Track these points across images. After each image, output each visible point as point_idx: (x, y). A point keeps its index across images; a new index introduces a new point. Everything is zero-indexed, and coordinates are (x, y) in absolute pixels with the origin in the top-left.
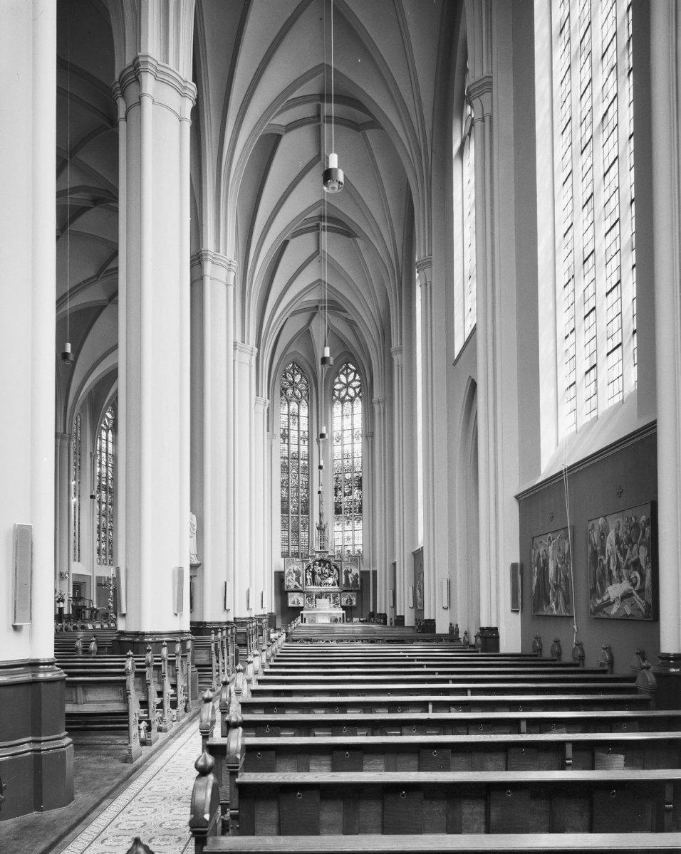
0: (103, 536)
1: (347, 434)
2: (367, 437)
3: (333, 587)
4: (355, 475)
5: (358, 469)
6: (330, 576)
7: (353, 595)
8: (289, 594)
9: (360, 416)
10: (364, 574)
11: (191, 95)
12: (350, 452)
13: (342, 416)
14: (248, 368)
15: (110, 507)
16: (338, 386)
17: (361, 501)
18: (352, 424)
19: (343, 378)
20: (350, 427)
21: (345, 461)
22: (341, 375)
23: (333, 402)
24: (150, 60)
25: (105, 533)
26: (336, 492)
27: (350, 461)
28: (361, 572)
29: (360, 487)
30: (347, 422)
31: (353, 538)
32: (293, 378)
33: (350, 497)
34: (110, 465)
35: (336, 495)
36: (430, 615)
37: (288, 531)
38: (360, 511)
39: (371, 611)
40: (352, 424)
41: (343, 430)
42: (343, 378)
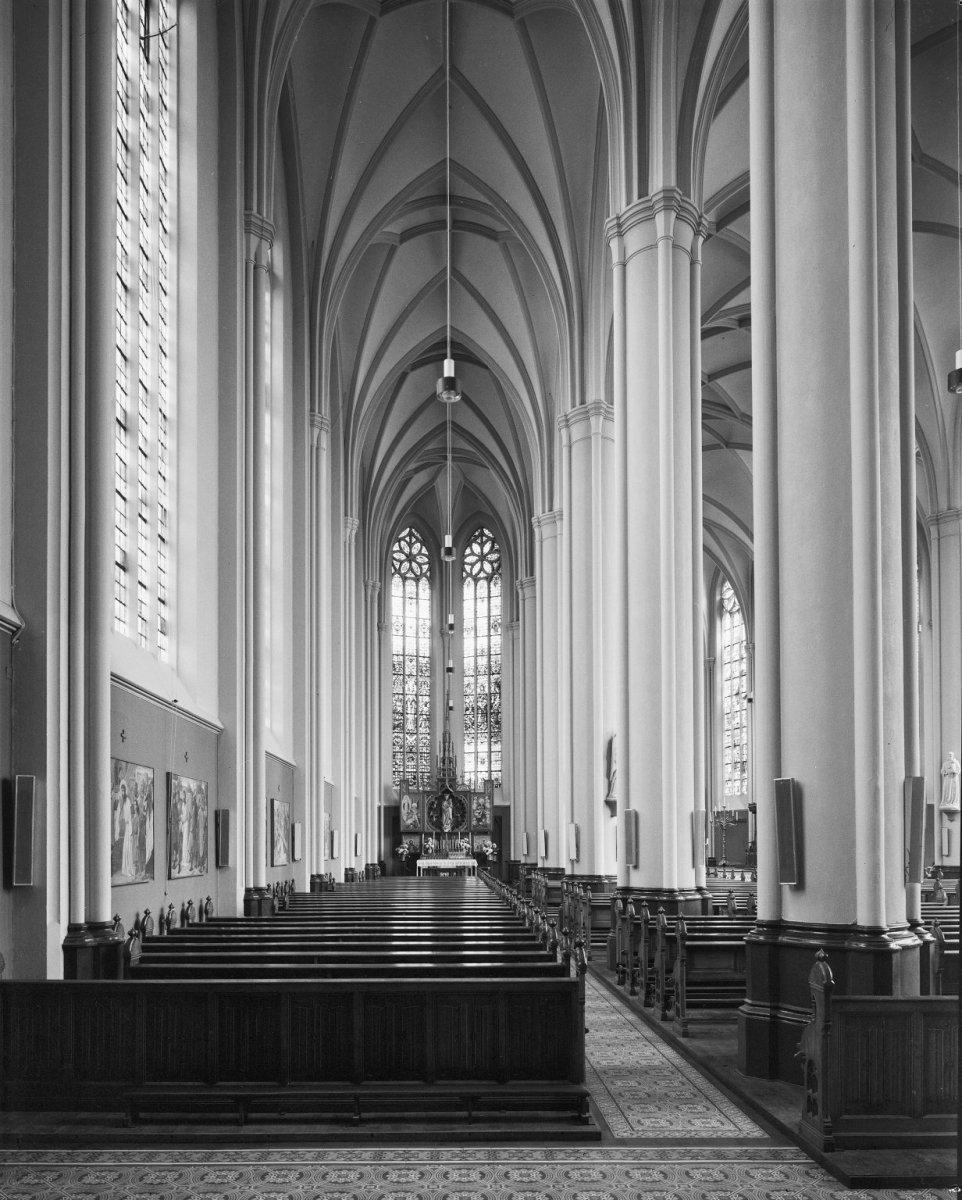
8: (78, 951)
9: (428, 603)
16: (469, 560)
19: (476, 548)
22: (403, 543)
23: (463, 580)
32: (410, 548)
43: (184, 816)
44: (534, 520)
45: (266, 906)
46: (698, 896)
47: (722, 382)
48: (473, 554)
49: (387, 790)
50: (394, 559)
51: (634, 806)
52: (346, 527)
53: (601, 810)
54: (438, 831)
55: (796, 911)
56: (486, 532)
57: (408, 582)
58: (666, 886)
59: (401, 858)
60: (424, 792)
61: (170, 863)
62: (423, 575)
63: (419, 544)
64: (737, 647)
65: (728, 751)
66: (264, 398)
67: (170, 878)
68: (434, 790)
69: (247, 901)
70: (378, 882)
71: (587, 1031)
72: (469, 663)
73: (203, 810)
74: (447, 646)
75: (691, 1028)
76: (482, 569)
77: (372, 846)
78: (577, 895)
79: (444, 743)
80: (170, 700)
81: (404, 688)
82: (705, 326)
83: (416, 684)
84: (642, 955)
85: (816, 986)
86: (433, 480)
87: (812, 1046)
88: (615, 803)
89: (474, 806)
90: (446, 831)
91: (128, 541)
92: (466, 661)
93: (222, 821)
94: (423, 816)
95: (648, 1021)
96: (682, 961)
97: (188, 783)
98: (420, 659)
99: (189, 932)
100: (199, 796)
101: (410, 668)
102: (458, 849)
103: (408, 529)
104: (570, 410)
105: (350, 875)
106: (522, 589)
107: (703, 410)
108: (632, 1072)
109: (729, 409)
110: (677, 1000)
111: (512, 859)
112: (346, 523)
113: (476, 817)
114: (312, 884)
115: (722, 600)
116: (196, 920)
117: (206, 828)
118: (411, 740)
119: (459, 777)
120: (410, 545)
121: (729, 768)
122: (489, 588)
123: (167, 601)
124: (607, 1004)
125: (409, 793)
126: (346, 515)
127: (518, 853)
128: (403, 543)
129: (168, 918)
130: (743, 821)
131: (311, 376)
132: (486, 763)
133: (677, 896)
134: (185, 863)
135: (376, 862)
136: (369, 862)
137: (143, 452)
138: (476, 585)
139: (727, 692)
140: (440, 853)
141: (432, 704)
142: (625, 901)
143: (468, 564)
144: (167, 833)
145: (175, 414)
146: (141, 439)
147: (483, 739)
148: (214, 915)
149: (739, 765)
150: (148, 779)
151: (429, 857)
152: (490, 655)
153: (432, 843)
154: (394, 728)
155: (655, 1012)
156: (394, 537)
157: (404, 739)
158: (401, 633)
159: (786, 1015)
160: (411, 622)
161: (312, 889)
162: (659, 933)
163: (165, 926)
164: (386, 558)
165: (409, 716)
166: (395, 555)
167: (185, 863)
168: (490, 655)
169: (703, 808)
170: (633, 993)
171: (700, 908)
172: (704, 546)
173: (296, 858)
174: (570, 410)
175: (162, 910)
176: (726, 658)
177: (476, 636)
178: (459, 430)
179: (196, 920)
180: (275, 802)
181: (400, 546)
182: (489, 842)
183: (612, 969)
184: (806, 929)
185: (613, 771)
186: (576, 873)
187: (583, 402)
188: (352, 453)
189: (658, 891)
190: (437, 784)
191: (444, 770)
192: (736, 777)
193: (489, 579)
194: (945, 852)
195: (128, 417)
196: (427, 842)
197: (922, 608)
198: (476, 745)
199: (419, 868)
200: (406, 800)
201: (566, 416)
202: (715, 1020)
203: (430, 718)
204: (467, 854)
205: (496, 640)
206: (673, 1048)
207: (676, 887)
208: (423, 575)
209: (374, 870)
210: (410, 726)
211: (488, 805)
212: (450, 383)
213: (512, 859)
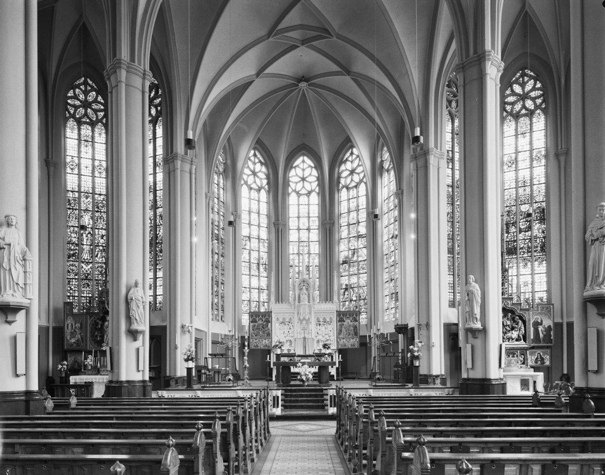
0: (215, 289)
1: (524, 157)
2: (557, 155)
3: (517, 343)
4: (535, 206)
5: (540, 198)
6: (513, 328)
7: (545, 353)
10: (558, 326)
12: (528, 178)
13: (516, 135)
14: (188, 175)
15: (222, 259)
17: (544, 237)
18: (531, 143)
20: (528, 148)
21: (521, 191)
24: (122, 61)
25: (218, 286)
26: (508, 228)
27: (528, 189)
28: (556, 324)
29: (542, 220)
30: (524, 142)
31: (533, 284)
33: (527, 234)
34: (221, 213)
35: (508, 232)
37: (453, 275)
38: (543, 248)
39: (565, 372)
40: (531, 143)
41: (517, 152)
42: (517, 89)
57: (83, 127)
62: (99, 121)
63: (94, 93)
64: (392, 198)
65: (387, 285)
83: (92, 218)
94: (86, 336)
98: (96, 196)
101: (86, 203)
103: (83, 79)
111: (168, 375)
118: (86, 268)
120: (86, 93)
121: (387, 299)
128: (77, 90)
149: (394, 295)
158: (76, 171)
160: (86, 163)
165: (85, 246)
173: (140, 369)
176: (385, 209)
192: (392, 306)
194: (593, 365)
197: (549, 143)
200: (69, 321)
208: (99, 121)
210: (86, 256)
213: (168, 375)
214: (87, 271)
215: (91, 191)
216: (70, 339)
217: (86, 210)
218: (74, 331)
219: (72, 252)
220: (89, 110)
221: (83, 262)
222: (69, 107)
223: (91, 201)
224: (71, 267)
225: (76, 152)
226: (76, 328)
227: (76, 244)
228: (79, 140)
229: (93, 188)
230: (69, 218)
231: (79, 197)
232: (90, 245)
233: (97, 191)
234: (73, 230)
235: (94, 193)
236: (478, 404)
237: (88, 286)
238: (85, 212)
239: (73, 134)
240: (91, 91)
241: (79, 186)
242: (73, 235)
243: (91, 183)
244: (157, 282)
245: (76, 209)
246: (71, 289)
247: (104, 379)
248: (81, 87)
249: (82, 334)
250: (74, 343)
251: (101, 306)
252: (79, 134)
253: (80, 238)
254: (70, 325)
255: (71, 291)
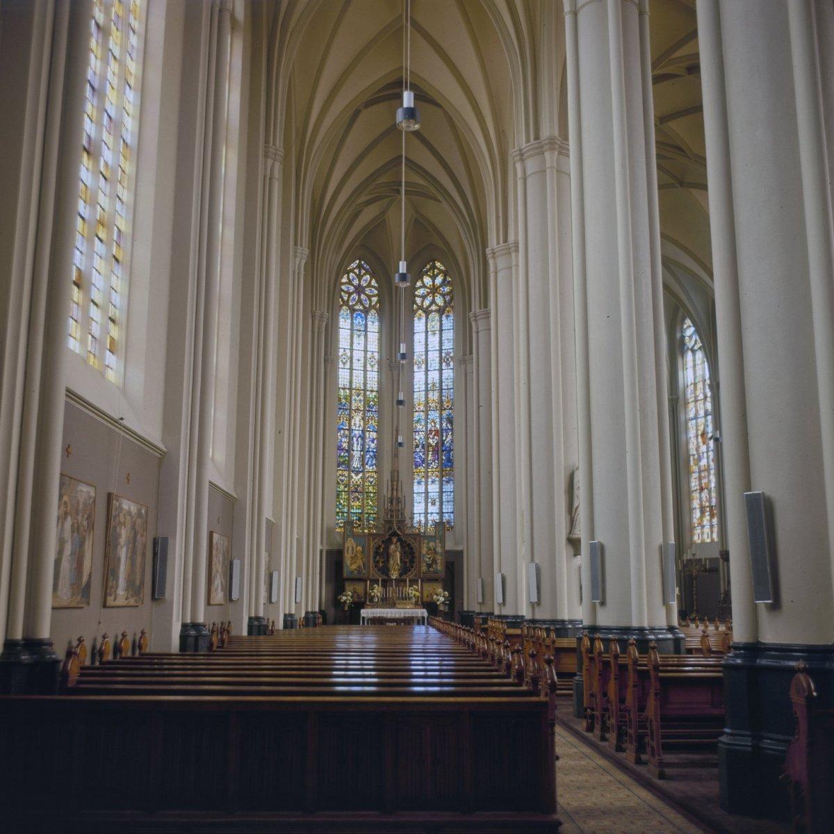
11: (282, 154)
16: (421, 292)
22: (351, 275)
32: (360, 281)
36: (312, 608)
43: (123, 540)
44: (488, 251)
45: (203, 644)
46: (670, 636)
47: (674, 125)
48: (424, 286)
49: (330, 531)
50: (343, 291)
51: (600, 538)
52: (295, 256)
53: (563, 549)
54: (385, 577)
55: (772, 634)
56: (438, 264)
58: (635, 624)
59: (344, 607)
60: (370, 534)
61: (106, 590)
62: (371, 307)
63: (368, 276)
66: (222, 134)
67: (105, 606)
68: (382, 532)
69: (184, 638)
70: (318, 630)
71: (558, 758)
72: (419, 397)
73: (142, 536)
74: (396, 378)
75: (668, 771)
76: (433, 302)
77: (313, 593)
78: (538, 638)
79: (392, 481)
80: (116, 417)
81: (350, 424)
82: (655, 73)
83: (363, 419)
84: (612, 695)
85: (797, 700)
86: (383, 213)
87: (798, 767)
88: (579, 541)
89: (424, 550)
90: (394, 577)
91: (84, 258)
92: (416, 396)
93: (160, 551)
94: (369, 562)
95: (621, 765)
96: (656, 694)
97: (128, 506)
98: (368, 393)
99: (118, 663)
100: (139, 521)
101: (357, 402)
102: (406, 598)
103: (358, 261)
104: (524, 145)
105: (289, 622)
106: (476, 320)
107: (657, 151)
108: (604, 812)
109: (681, 150)
110: (652, 739)
111: (465, 609)
112: (295, 252)
113: (426, 562)
114: (250, 627)
115: (683, 337)
116: (129, 654)
117: (144, 555)
118: (356, 478)
119: (407, 519)
120: (359, 277)
122: (441, 321)
123: (117, 320)
124: (575, 750)
125: (354, 536)
126: (296, 244)
127: (471, 602)
129: (101, 648)
130: (714, 570)
131: (267, 112)
132: (437, 504)
133: (647, 635)
134: (121, 592)
135: (317, 610)
136: (310, 610)
137: (103, 176)
138: (427, 318)
139: (692, 433)
140: (386, 602)
141: (379, 440)
142: (592, 640)
143: (419, 296)
144: (105, 557)
145: (136, 142)
146: (102, 163)
147: (434, 476)
148: (147, 651)
150: (90, 497)
151: (374, 605)
152: (441, 389)
153: (377, 591)
154: (339, 466)
155: (629, 756)
156: (342, 270)
157: (350, 477)
159: (769, 744)
160: (359, 355)
161: (250, 632)
162: (630, 668)
163: (98, 658)
164: (335, 289)
166: (343, 287)
167: (121, 592)
168: (441, 389)
169: (672, 541)
170: (603, 739)
171: (672, 649)
172: (664, 284)
174: (524, 145)
175: (95, 640)
177: (427, 370)
178: (412, 165)
179: (129, 654)
180: (214, 534)
181: (348, 278)
182: (440, 590)
183: (579, 717)
184: (785, 651)
185: (575, 506)
186: (538, 617)
187: (537, 137)
188: (304, 183)
189: (627, 630)
190: (384, 526)
191: (391, 511)
193: (441, 311)
195: (92, 142)
196: (372, 589)
198: (426, 485)
199: (363, 618)
200: (350, 543)
201: (520, 150)
202: (693, 764)
203: (377, 456)
204: (416, 604)
205: (448, 373)
206: (649, 790)
207: (646, 625)
208: (371, 307)
209: (315, 618)
210: (356, 464)
211: (439, 550)
212: (411, 113)
213: (465, 609)
214: (357, 482)
215: (362, 388)
216: (351, 565)
217: (358, 410)
218: (355, 555)
219: (342, 460)
220: (363, 296)
221: (353, 471)
222: (343, 293)
223: (362, 399)
224: (341, 477)
225: (349, 344)
226: (356, 551)
227: (346, 450)
228: (352, 329)
229: (365, 384)
230: (340, 419)
231: (351, 396)
232: (361, 451)
233: (369, 387)
234: (344, 434)
235: (365, 390)
236: (189, 687)
237: (358, 499)
238: (356, 412)
239: (346, 324)
240: (365, 274)
241: (351, 382)
242: (344, 440)
243: (362, 379)
244: (444, 497)
245: (347, 409)
246: (341, 504)
247: (400, 613)
248: (436, 270)
249: (364, 560)
250: (355, 569)
251: (387, 527)
252: (352, 324)
253: (350, 444)
254: (350, 548)
255: (340, 507)
